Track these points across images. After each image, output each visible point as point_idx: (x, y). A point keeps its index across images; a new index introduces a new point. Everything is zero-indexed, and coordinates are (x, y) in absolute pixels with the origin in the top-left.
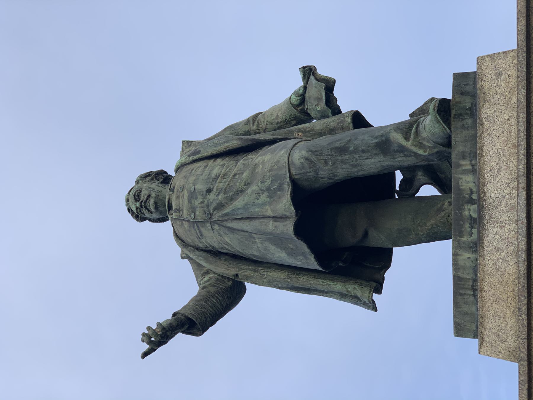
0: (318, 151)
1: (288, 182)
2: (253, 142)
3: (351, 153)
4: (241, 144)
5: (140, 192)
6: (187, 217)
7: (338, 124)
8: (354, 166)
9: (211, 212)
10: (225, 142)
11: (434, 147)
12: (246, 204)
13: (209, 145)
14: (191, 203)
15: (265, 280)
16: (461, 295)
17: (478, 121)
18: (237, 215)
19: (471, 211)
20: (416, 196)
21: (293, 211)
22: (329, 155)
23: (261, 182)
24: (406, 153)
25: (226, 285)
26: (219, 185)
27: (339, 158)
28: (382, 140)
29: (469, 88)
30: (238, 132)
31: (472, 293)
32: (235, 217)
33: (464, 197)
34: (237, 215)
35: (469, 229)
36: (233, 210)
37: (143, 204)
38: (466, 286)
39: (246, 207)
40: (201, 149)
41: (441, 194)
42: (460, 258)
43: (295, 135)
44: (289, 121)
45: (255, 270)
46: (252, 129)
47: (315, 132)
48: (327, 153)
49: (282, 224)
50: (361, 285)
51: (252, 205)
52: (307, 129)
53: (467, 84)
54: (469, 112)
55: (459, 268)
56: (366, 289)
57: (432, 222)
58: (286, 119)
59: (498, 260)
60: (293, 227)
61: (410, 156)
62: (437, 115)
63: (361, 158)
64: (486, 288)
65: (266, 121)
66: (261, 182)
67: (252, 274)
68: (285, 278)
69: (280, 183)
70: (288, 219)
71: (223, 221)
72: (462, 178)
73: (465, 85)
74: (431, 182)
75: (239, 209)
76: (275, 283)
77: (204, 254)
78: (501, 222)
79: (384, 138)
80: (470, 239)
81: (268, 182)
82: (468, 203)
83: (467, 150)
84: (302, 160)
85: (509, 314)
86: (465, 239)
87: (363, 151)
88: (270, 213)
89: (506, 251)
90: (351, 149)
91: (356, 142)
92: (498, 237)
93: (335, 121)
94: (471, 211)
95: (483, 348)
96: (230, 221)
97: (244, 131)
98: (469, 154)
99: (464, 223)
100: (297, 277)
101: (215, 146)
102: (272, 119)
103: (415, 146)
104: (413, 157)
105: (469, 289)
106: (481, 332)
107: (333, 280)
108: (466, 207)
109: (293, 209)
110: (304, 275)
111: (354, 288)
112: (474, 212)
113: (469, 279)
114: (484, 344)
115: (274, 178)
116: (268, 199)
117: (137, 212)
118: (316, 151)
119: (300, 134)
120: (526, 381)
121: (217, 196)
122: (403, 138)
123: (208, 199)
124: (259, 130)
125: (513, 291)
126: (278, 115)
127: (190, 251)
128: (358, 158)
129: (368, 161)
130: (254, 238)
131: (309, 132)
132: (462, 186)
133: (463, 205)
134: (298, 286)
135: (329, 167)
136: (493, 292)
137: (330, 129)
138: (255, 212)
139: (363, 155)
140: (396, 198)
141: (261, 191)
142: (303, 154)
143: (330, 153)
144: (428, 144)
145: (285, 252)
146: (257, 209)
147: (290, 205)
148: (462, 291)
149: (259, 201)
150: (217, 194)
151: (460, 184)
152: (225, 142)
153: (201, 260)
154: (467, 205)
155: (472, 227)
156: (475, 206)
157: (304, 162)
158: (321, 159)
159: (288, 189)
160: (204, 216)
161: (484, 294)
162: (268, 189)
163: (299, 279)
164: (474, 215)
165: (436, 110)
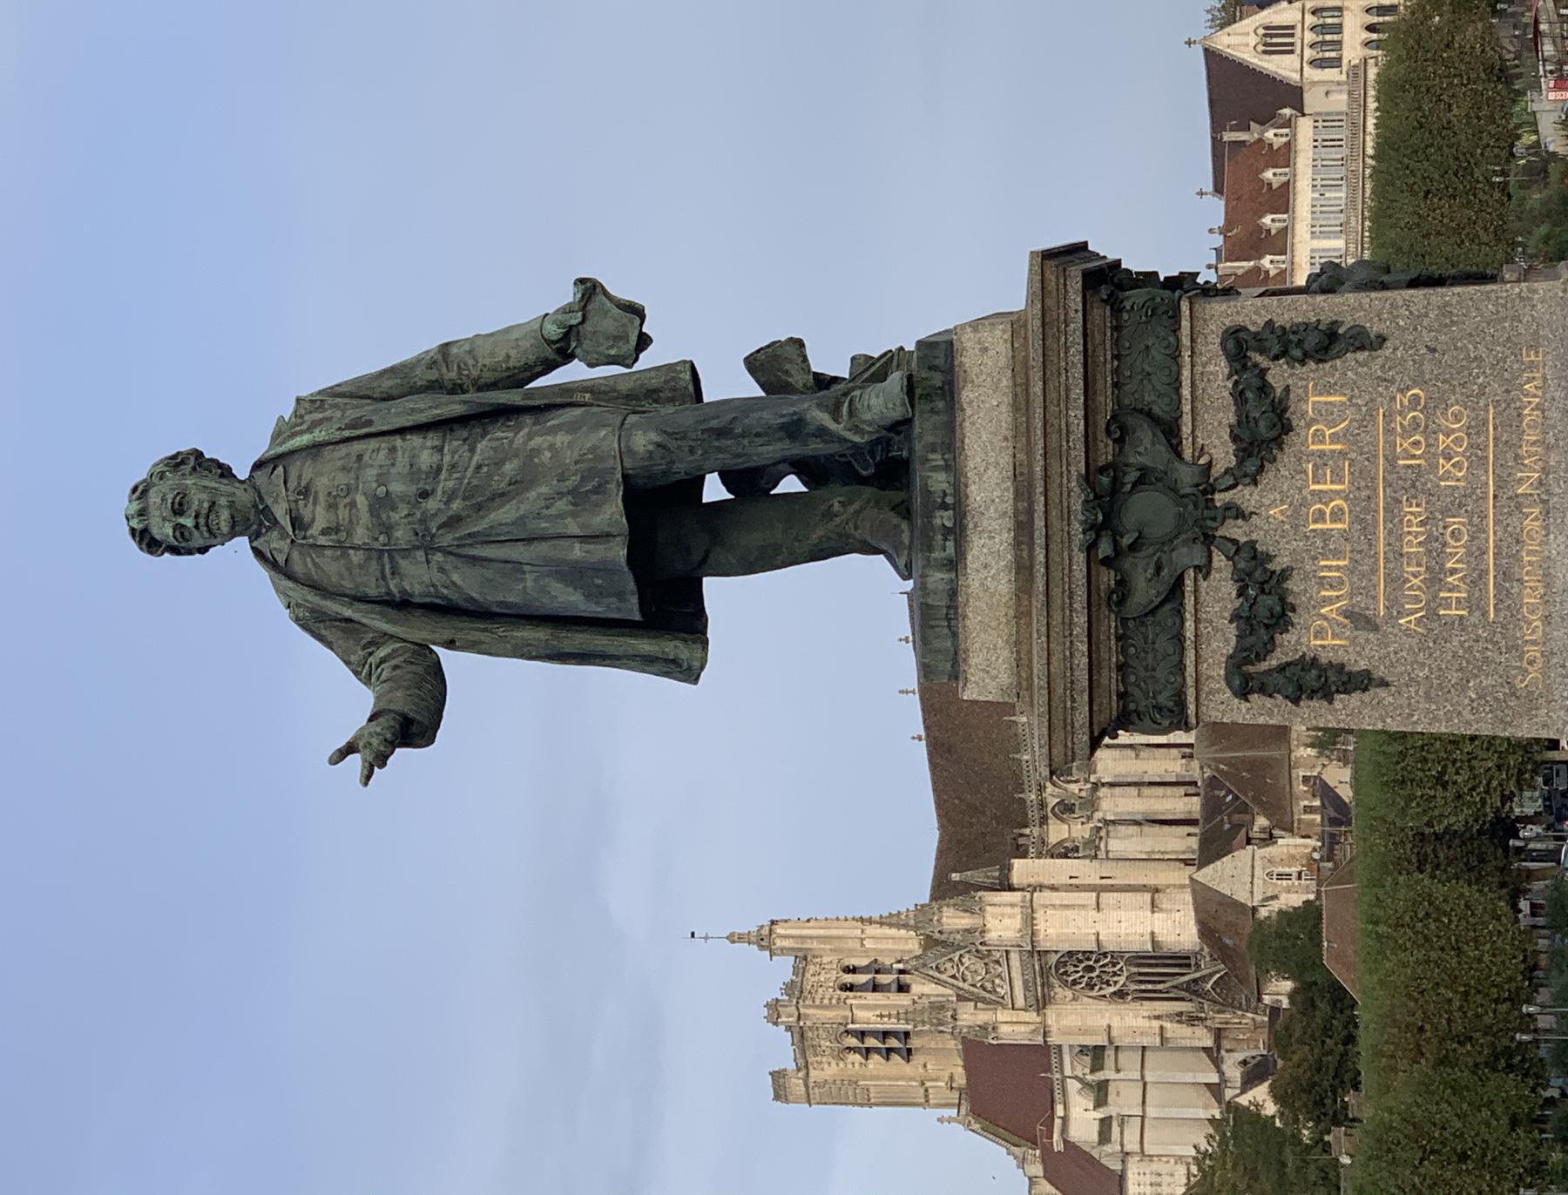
0: (677, 434)
2: (491, 408)
3: (736, 437)
8: (739, 456)
11: (877, 432)
12: (522, 518)
13: (393, 410)
15: (509, 646)
17: (957, 406)
19: (944, 518)
20: (773, 492)
24: (826, 438)
26: (446, 483)
29: (940, 362)
32: (492, 539)
33: (935, 501)
34: (500, 535)
35: (941, 542)
39: (520, 521)
41: (806, 490)
42: (929, 579)
45: (485, 630)
54: (939, 392)
56: (694, 646)
57: (820, 532)
59: (986, 578)
60: (626, 551)
64: (970, 615)
67: (483, 636)
68: (547, 640)
74: (792, 470)
77: (378, 608)
78: (990, 532)
80: (943, 555)
84: (651, 448)
85: (1000, 643)
87: (758, 435)
88: (576, 531)
89: (996, 567)
90: (737, 431)
92: (985, 550)
94: (944, 518)
101: (409, 415)
111: (676, 646)
112: (949, 519)
114: (968, 685)
115: (586, 474)
116: (571, 507)
117: (174, 537)
118: (674, 433)
120: (1046, 712)
121: (448, 502)
125: (1006, 615)
126: (508, 357)
130: (524, 572)
131: (605, 393)
135: (696, 457)
136: (980, 618)
139: (756, 439)
143: (700, 437)
144: (867, 428)
149: (552, 511)
152: (430, 407)
155: (946, 540)
161: (968, 622)
162: (573, 492)
164: (949, 524)
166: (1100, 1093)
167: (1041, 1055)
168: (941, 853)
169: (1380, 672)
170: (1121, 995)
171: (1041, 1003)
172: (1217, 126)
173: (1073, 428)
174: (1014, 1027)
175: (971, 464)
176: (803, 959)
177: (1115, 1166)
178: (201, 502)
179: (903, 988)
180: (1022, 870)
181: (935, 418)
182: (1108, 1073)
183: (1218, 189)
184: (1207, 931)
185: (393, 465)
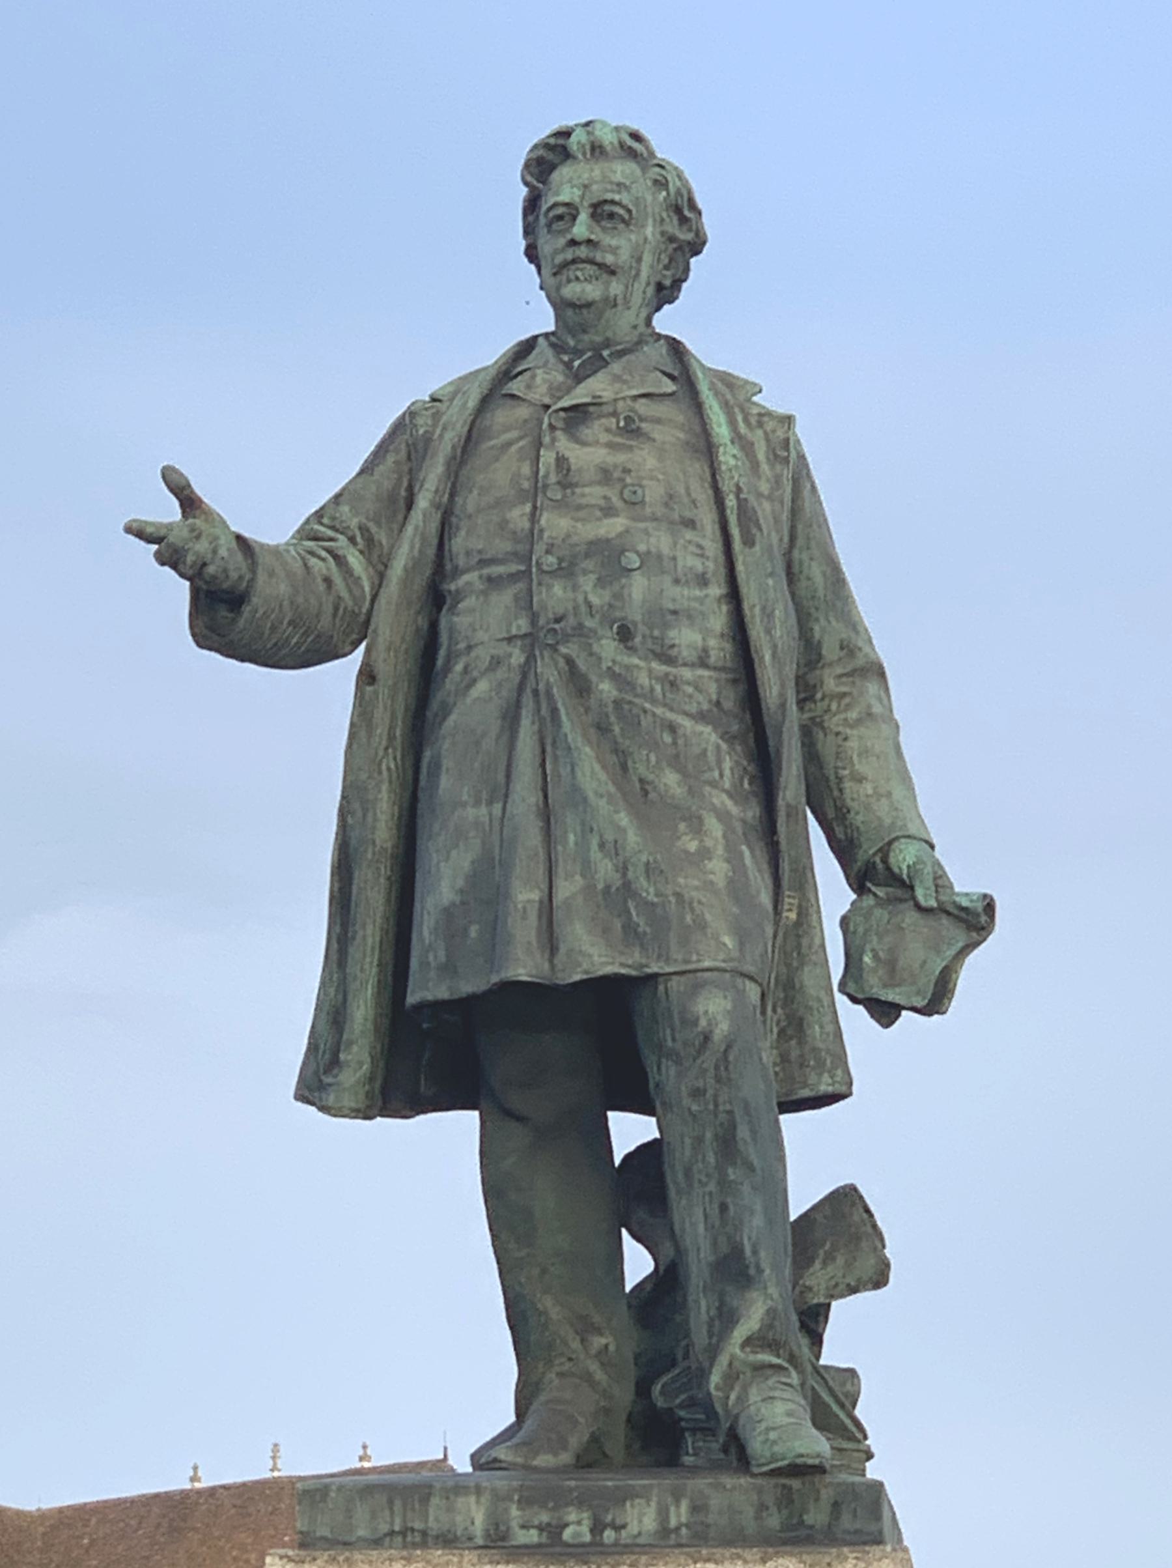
0: (726, 1069)
1: (647, 966)
2: (773, 755)
3: (721, 1169)
4: (768, 709)
5: (623, 221)
6: (546, 535)
7: (815, 1049)
9: (563, 650)
10: (775, 646)
11: (727, 1411)
14: (587, 555)
15: (364, 776)
16: (391, 1502)
17: (770, 1550)
18: (556, 758)
20: (624, 1232)
21: (570, 977)
22: (716, 1105)
23: (648, 861)
24: (717, 1323)
25: (340, 644)
27: (709, 1135)
28: (747, 1267)
29: (846, 1522)
30: (817, 620)
31: (397, 1528)
32: (549, 749)
33: (607, 1510)
34: (556, 758)
35: (536, 1523)
36: (569, 748)
37: (582, 252)
38: (409, 1514)
39: (577, 798)
40: (757, 548)
43: (789, 897)
44: (844, 818)
45: (391, 738)
46: (827, 671)
47: (797, 969)
48: (721, 1100)
49: (533, 938)
50: (371, 1079)
51: (583, 824)
52: (805, 942)
53: (855, 1516)
54: (795, 1521)
55: (448, 1498)
58: (849, 811)
61: (711, 1335)
62: (786, 1462)
63: (707, 1198)
65: (849, 731)
66: (648, 861)
67: (381, 730)
69: (645, 933)
70: (547, 955)
71: (536, 693)
72: (649, 1505)
73: (855, 1510)
75: (573, 770)
76: (356, 806)
79: (752, 1271)
80: (514, 1524)
81: (649, 892)
82: (595, 1519)
83: (711, 1518)
84: (703, 1023)
86: (514, 1512)
87: (723, 1208)
88: (565, 889)
90: (730, 1171)
91: (746, 1188)
93: (824, 1036)
95: (280, 1563)
96: (536, 727)
97: (819, 642)
98: (702, 1523)
99: (550, 1510)
100: (382, 880)
102: (851, 758)
103: (730, 1364)
104: (707, 1341)
105: (404, 1521)
106: (315, 1559)
108: (585, 1515)
109: (577, 977)
110: (388, 901)
112: (577, 1535)
113: (426, 1522)
115: (659, 911)
116: (600, 886)
117: (555, 205)
119: (793, 916)
122: (750, 1333)
123: (600, 632)
124: (823, 699)
127: (436, 491)
128: (707, 1189)
129: (699, 1213)
131: (799, 946)
132: (632, 1506)
133: (590, 1507)
134: (355, 882)
137: (801, 1019)
138: (566, 832)
139: (716, 1206)
141: (624, 863)
142: (720, 1026)
143: (721, 1108)
145: (453, 904)
146: (571, 838)
147: (586, 972)
148: (398, 1504)
149: (595, 854)
150: (617, 669)
151: (637, 1501)
152: (775, 646)
153: (412, 547)
154: (589, 1518)
155: (541, 1528)
156: (587, 1538)
157: (699, 1029)
158: (708, 1080)
159: (629, 966)
160: (551, 616)
162: (627, 888)
163: (376, 889)
164: (567, 1534)
165: (799, 1461)
178: (614, 250)
181: (750, 1512)
185: (677, 581)
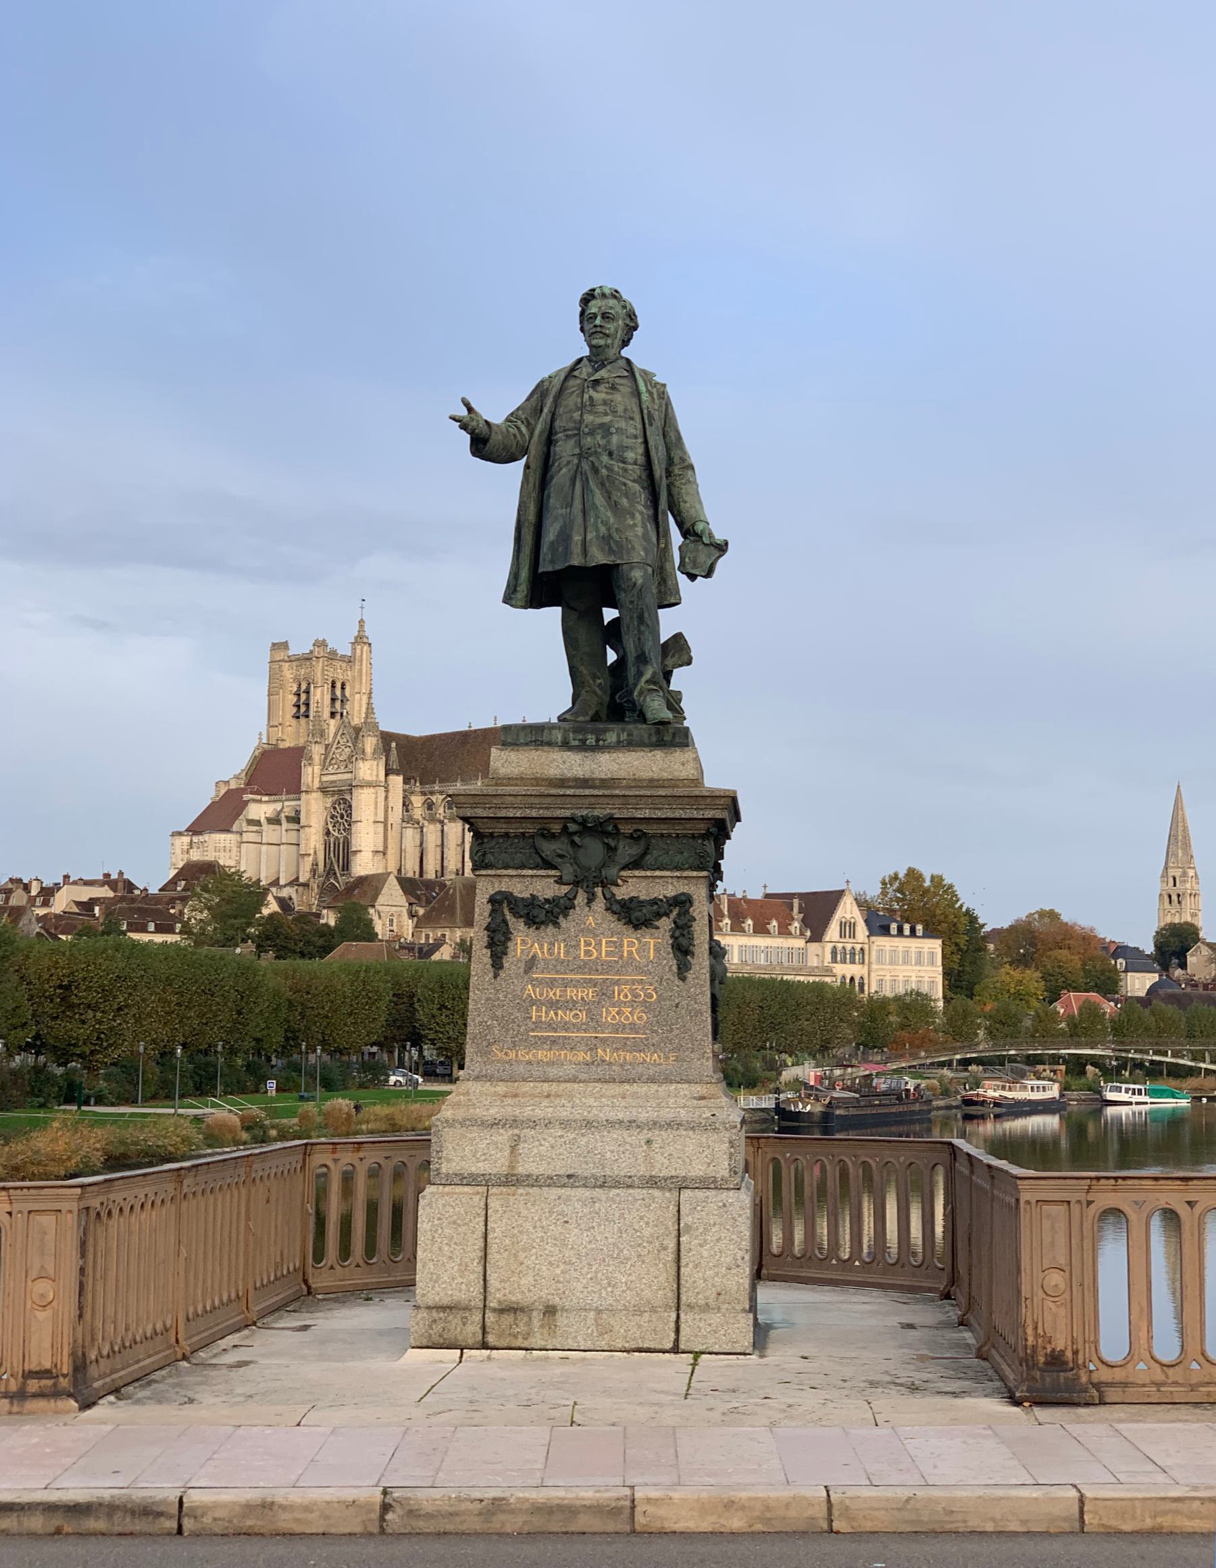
8: (628, 628)
19: (591, 740)
29: (677, 740)
37: (599, 329)
45: (535, 487)
50: (526, 596)
67: (531, 485)
77: (548, 427)
83: (634, 738)
86: (571, 735)
87: (639, 639)
88: (589, 537)
91: (647, 633)
94: (591, 740)
107: (529, 569)
126: (686, 502)
140: (604, 609)
149: (600, 525)
155: (579, 740)
162: (610, 536)
164: (588, 743)
166: (274, 821)
167: (295, 789)
168: (407, 737)
169: (502, 974)
170: (328, 833)
171: (323, 790)
172: (802, 896)
173: (639, 812)
174: (311, 775)
175: (620, 755)
176: (350, 661)
177: (235, 828)
178: (609, 329)
179: (333, 715)
180: (397, 781)
182: (285, 825)
183: (767, 896)
184: (362, 880)
